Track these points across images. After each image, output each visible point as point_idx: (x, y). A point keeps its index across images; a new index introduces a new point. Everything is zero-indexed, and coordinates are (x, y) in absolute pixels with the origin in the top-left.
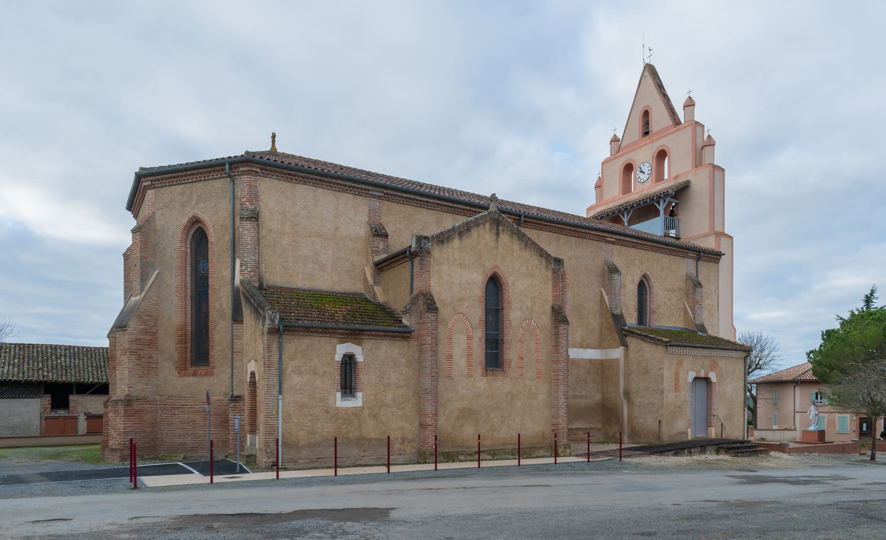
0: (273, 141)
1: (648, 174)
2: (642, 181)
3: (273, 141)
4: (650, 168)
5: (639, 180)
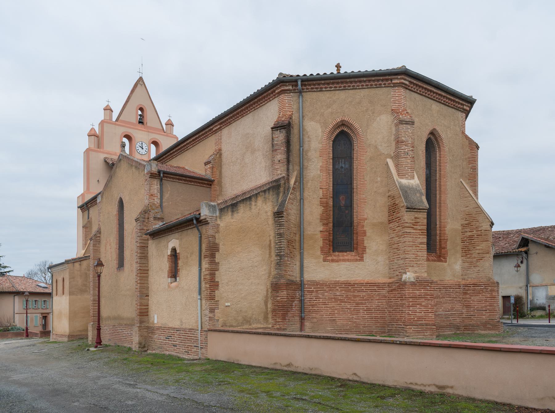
1: (146, 151)
2: (141, 153)
5: (138, 151)
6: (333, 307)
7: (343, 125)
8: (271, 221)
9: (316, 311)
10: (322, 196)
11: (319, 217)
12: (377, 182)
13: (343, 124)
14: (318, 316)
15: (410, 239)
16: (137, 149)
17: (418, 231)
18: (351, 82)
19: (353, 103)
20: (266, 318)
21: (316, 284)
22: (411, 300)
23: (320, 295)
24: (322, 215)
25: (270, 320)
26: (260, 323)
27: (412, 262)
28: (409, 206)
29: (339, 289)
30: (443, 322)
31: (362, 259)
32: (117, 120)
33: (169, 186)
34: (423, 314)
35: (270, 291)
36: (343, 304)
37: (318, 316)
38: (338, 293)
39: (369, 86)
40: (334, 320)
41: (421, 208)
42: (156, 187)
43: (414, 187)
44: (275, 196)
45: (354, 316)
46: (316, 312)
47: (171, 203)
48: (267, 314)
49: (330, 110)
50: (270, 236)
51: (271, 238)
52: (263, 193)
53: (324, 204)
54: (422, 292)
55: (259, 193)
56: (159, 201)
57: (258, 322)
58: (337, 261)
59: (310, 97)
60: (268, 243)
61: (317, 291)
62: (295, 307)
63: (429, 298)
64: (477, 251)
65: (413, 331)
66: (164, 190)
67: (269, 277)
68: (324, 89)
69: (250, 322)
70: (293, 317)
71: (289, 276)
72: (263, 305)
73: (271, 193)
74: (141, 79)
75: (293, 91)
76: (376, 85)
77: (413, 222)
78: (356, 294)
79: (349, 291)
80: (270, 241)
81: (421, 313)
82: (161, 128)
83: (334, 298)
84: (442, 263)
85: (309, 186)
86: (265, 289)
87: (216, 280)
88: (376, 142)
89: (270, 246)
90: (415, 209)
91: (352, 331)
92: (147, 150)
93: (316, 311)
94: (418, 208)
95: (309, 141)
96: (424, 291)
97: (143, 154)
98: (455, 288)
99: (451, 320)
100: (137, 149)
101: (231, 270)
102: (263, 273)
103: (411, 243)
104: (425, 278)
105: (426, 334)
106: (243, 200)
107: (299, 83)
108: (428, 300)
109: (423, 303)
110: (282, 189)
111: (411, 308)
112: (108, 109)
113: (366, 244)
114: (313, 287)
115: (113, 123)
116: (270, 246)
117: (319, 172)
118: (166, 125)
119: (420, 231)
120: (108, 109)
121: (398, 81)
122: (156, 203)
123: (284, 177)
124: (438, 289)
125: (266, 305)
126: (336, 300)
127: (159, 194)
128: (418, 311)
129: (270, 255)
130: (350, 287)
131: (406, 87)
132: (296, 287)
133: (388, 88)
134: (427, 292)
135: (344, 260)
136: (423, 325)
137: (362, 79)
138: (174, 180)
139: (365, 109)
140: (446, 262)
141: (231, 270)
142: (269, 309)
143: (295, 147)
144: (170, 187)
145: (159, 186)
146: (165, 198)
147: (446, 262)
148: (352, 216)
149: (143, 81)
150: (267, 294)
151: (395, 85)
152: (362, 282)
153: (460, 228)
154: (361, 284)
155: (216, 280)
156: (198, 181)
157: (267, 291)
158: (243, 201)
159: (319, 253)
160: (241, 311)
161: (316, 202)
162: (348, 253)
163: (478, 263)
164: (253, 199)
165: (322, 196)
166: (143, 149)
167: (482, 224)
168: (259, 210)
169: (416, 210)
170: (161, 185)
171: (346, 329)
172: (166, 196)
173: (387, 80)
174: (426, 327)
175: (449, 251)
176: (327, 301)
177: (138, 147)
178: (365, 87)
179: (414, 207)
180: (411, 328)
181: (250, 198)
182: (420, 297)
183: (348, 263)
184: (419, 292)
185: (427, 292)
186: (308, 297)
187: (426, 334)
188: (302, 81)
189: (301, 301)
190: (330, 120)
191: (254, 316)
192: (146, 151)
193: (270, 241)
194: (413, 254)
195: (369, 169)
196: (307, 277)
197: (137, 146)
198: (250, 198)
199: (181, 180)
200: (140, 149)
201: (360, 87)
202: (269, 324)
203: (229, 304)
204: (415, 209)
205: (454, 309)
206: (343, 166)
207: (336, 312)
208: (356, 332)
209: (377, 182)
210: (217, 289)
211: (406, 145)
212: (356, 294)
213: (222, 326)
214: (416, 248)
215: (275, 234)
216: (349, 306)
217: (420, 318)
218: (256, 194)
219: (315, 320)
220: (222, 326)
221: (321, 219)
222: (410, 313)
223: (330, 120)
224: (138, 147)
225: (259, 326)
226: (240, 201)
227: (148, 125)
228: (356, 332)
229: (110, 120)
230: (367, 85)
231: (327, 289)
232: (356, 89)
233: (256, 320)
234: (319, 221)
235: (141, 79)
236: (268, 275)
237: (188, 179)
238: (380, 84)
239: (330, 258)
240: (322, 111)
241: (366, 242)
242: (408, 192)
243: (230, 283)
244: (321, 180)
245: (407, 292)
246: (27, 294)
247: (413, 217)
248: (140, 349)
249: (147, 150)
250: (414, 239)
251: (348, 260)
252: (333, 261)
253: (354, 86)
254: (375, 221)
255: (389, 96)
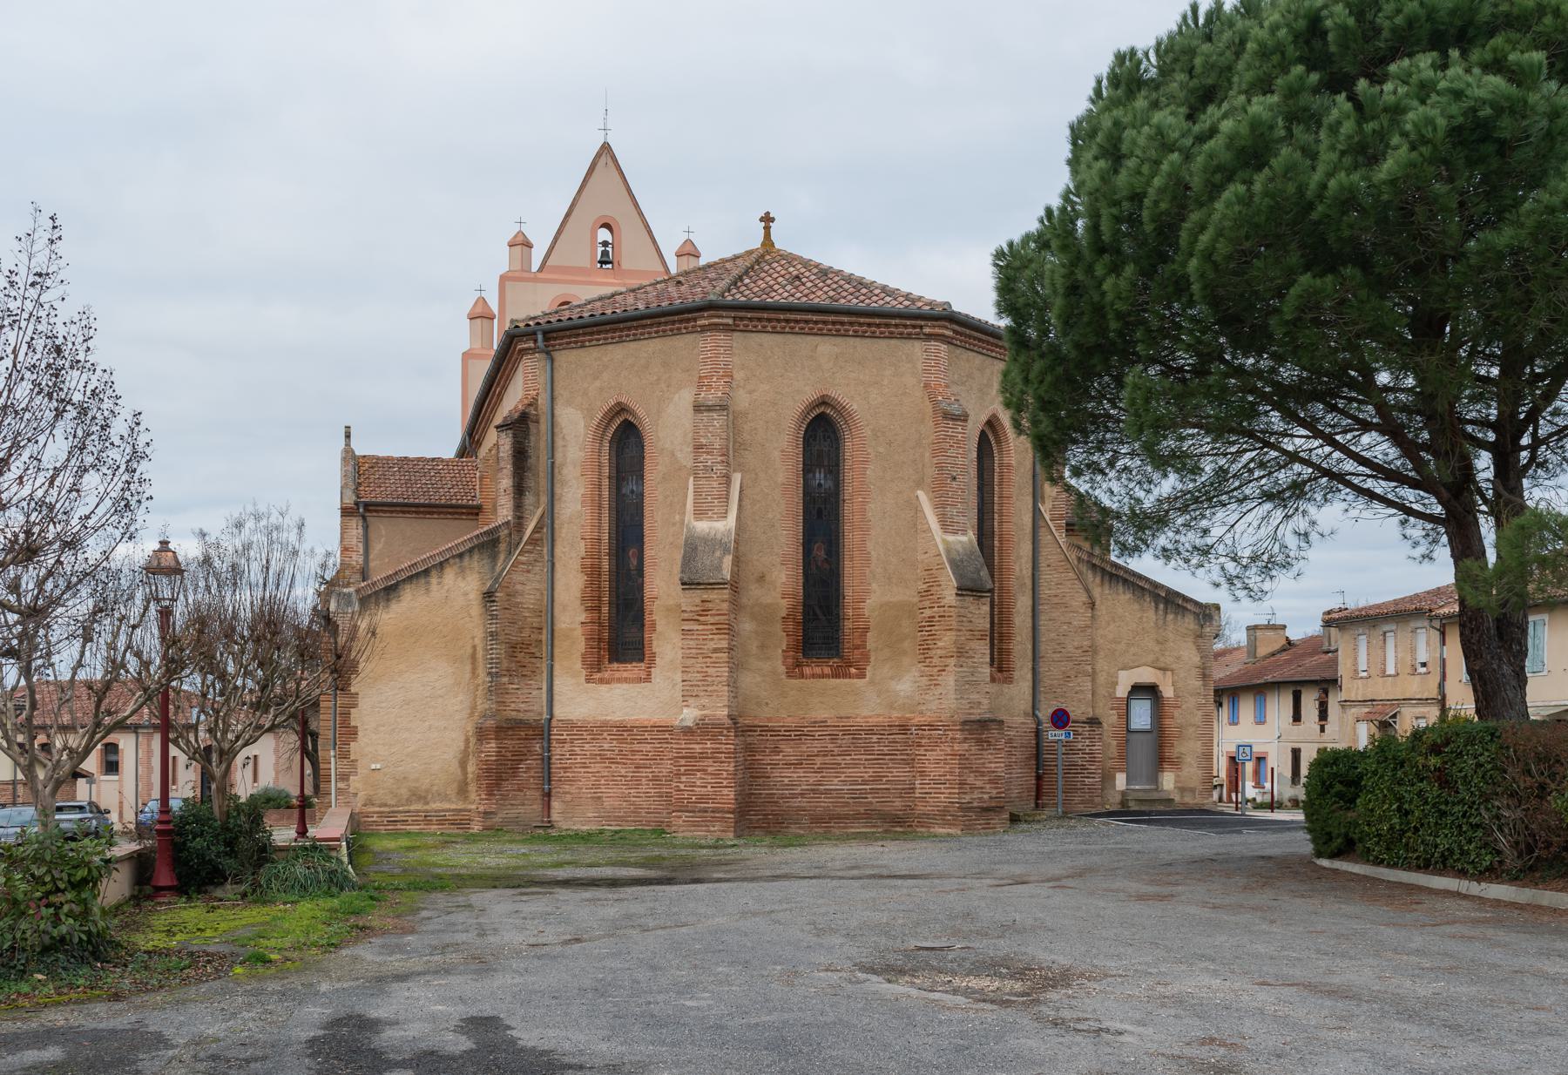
0: (767, 229)
3: (767, 229)
6: (598, 772)
7: (618, 413)
8: (476, 609)
9: (570, 781)
10: (583, 554)
11: (579, 595)
12: (674, 524)
13: (621, 409)
14: (573, 790)
15: (691, 642)
17: (710, 627)
18: (629, 329)
19: (636, 368)
20: (462, 791)
21: (571, 725)
22: (683, 762)
24: (584, 592)
25: (473, 796)
26: (450, 801)
27: (696, 689)
28: (685, 580)
29: (609, 737)
30: (843, 807)
31: (648, 679)
32: (541, 269)
33: (382, 527)
34: (709, 789)
35: (473, 740)
36: (613, 766)
37: (573, 790)
38: (606, 746)
39: (675, 332)
40: (599, 798)
41: (711, 581)
42: (355, 532)
43: (719, 537)
44: (485, 561)
45: (632, 791)
46: (572, 781)
47: (387, 560)
48: (467, 784)
49: (598, 383)
50: (473, 638)
51: (477, 641)
52: (457, 560)
53: (593, 572)
54: (709, 746)
55: (447, 560)
56: (361, 560)
57: (445, 798)
58: (608, 682)
59: (566, 359)
60: (469, 650)
61: (572, 741)
62: (525, 772)
63: (723, 759)
64: (939, 652)
65: (684, 821)
66: (372, 535)
67: (472, 714)
68: (587, 344)
69: (425, 798)
70: (519, 790)
71: (514, 713)
72: (454, 767)
73: (476, 557)
74: (606, 148)
75: (534, 350)
76: (671, 330)
77: (698, 608)
78: (636, 747)
79: (623, 741)
80: (474, 647)
81: (706, 787)
83: (600, 755)
84: (847, 681)
85: (563, 535)
86: (463, 738)
87: (353, 724)
88: (672, 443)
89: (473, 657)
90: (699, 584)
91: (627, 821)
93: (570, 781)
94: (706, 581)
95: (564, 446)
96: (713, 746)
98: (886, 733)
99: (871, 803)
101: (383, 705)
102: (456, 708)
103: (694, 651)
104: (719, 719)
105: (712, 829)
106: (410, 578)
107: (540, 337)
108: (721, 762)
109: (710, 769)
110: (503, 547)
111: (684, 779)
112: (522, 243)
113: (655, 649)
114: (565, 733)
115: (535, 280)
116: (473, 657)
117: (579, 507)
118: (678, 256)
119: (714, 627)
120: (522, 243)
121: (707, 322)
122: (354, 563)
123: (508, 523)
124: (827, 737)
125: (463, 765)
126: (604, 758)
127: (361, 545)
128: (698, 784)
129: (473, 673)
130: (625, 733)
131: (727, 329)
132: (531, 733)
133: (694, 335)
134: (718, 746)
135: (619, 680)
136: (706, 812)
137: (644, 322)
138: (394, 515)
139: (655, 378)
140: (862, 676)
141: (383, 705)
142: (470, 776)
143: (538, 458)
144: (383, 528)
145: (360, 531)
146: (376, 552)
147: (862, 676)
148: (641, 588)
150: (467, 747)
151: (704, 329)
152: (646, 723)
153: (916, 599)
154: (644, 728)
155: (353, 724)
156: (445, 510)
157: (467, 741)
158: (410, 578)
159: (579, 665)
160: (405, 778)
161: (575, 565)
162: (634, 664)
163: (939, 678)
164: (434, 573)
165: (583, 554)
167: (945, 592)
168: (448, 591)
169: (702, 587)
170: (366, 528)
171: (619, 817)
172: (377, 547)
173: (688, 320)
174: (712, 815)
175: (872, 654)
176: (587, 761)
178: (654, 335)
179: (696, 581)
180: (680, 817)
181: (426, 572)
182: (703, 756)
183: (625, 686)
184: (701, 746)
185: (718, 746)
186: (557, 751)
187: (712, 829)
188: (545, 333)
189: (547, 762)
190: (599, 403)
191: (435, 788)
193: (474, 647)
194: (698, 672)
195: (660, 498)
196: (560, 712)
198: (426, 572)
199: (409, 512)
201: (646, 336)
202: (473, 803)
203: (378, 767)
204: (699, 584)
205: (884, 779)
206: (635, 488)
207: (603, 782)
208: (635, 822)
209: (674, 524)
210: (355, 740)
211: (708, 453)
212: (636, 747)
213: (365, 805)
214: (705, 660)
215: (486, 632)
216: (623, 772)
217: (702, 798)
218: (441, 563)
219: (568, 797)
220: (365, 805)
221: (583, 599)
222: (682, 786)
223: (599, 403)
225: (447, 806)
226: (404, 580)
227: (625, 265)
228: (635, 822)
229: (523, 270)
230: (657, 332)
231: (589, 737)
232: (640, 339)
233: (439, 795)
234: (579, 602)
235: (606, 148)
236: (469, 711)
237: (422, 509)
238: (679, 329)
239: (598, 676)
240: (586, 385)
241: (655, 643)
242: (700, 548)
243: (382, 728)
244: (583, 523)
245: (674, 746)
247: (698, 601)
250: (701, 642)
251: (626, 680)
252: (602, 681)
253: (634, 335)
254: (671, 602)
255: (696, 351)
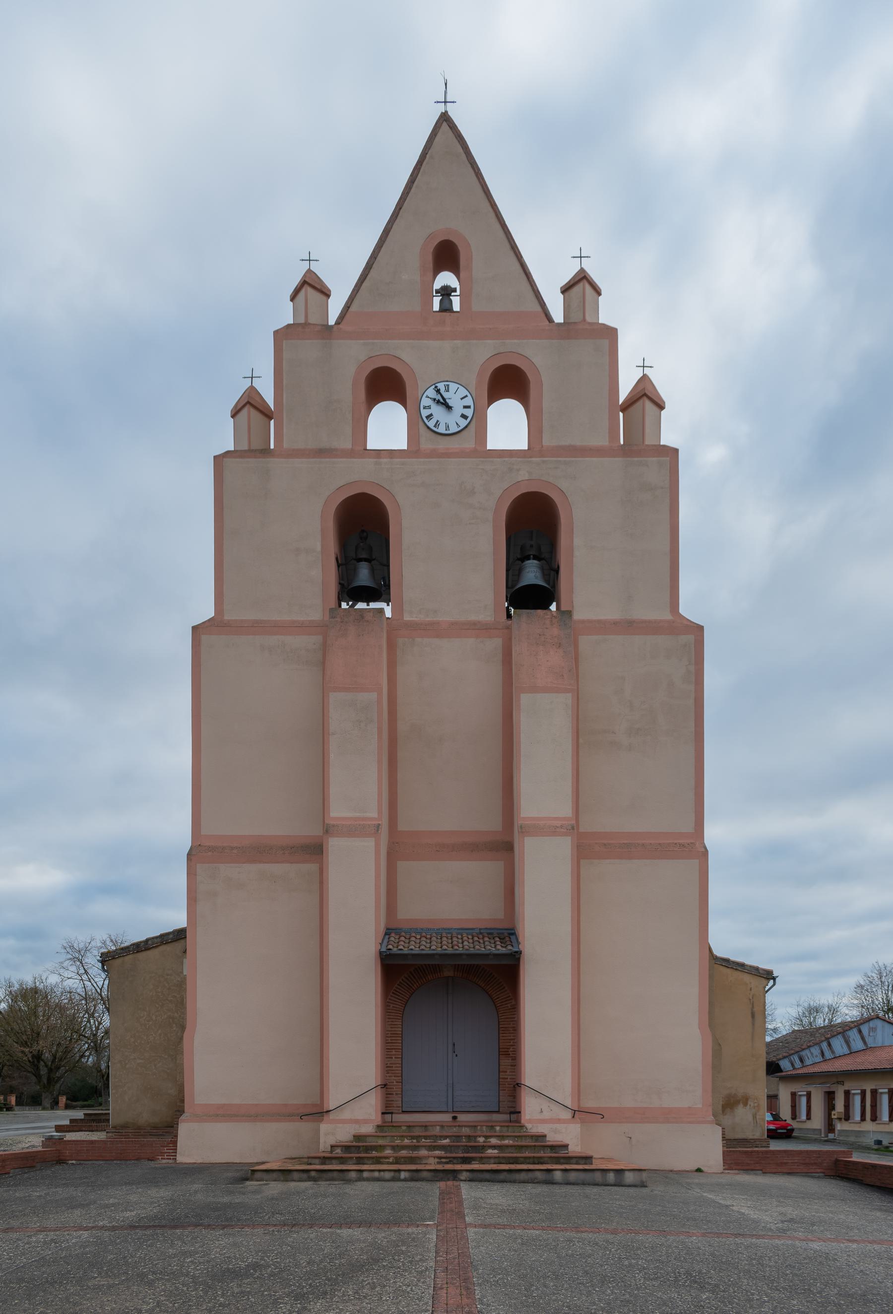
1: (464, 416)
2: (442, 429)
4: (469, 401)
5: (431, 424)
16: (425, 413)
23: (132, 1136)
48: (442, 1162)
74: (445, 118)
82: (539, 309)
92: (469, 413)
97: (453, 429)
100: (425, 413)
149: (453, 127)
166: (449, 408)
177: (429, 407)
192: (464, 416)
197: (425, 402)
200: (438, 412)
224: (429, 407)
235: (445, 118)
246: (448, 973)
248: (725, 1148)
249: (469, 413)
